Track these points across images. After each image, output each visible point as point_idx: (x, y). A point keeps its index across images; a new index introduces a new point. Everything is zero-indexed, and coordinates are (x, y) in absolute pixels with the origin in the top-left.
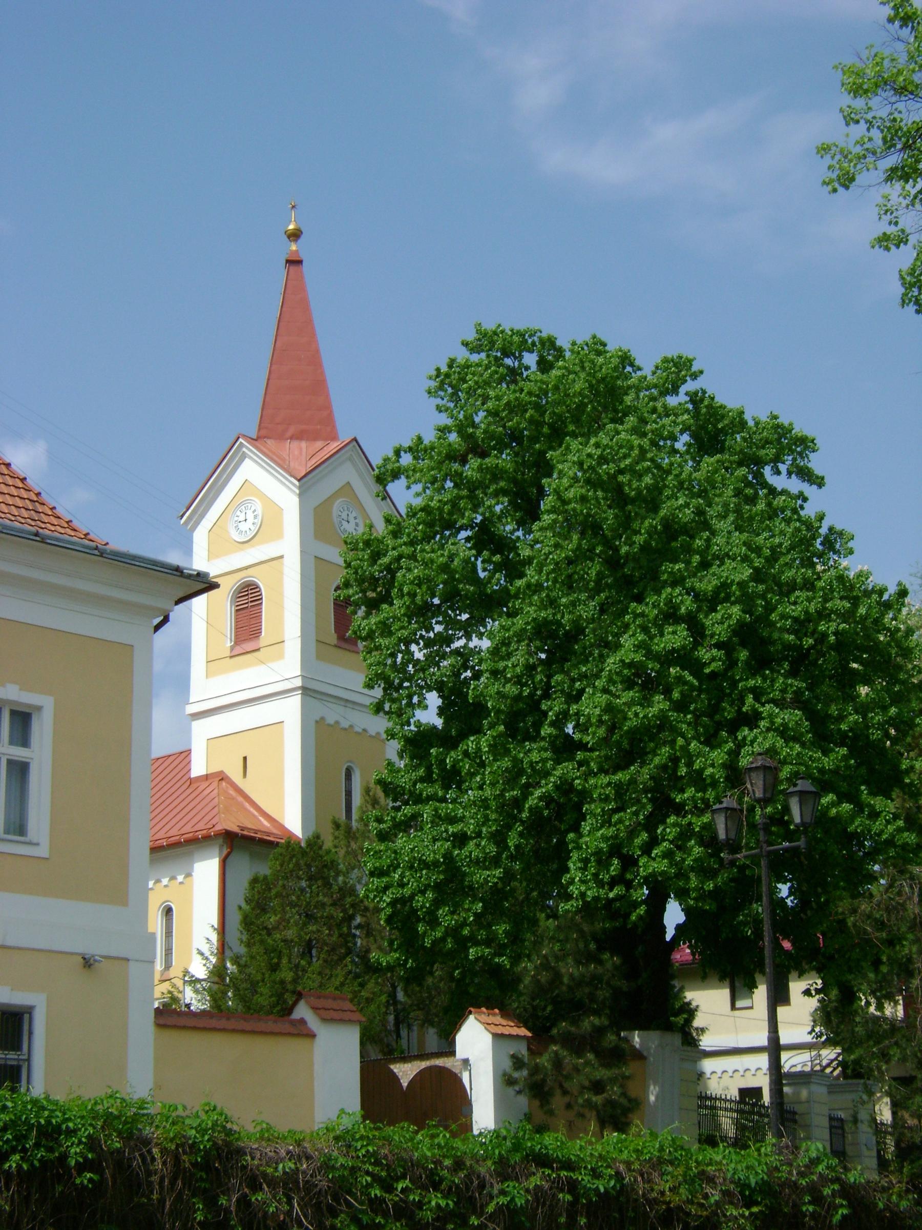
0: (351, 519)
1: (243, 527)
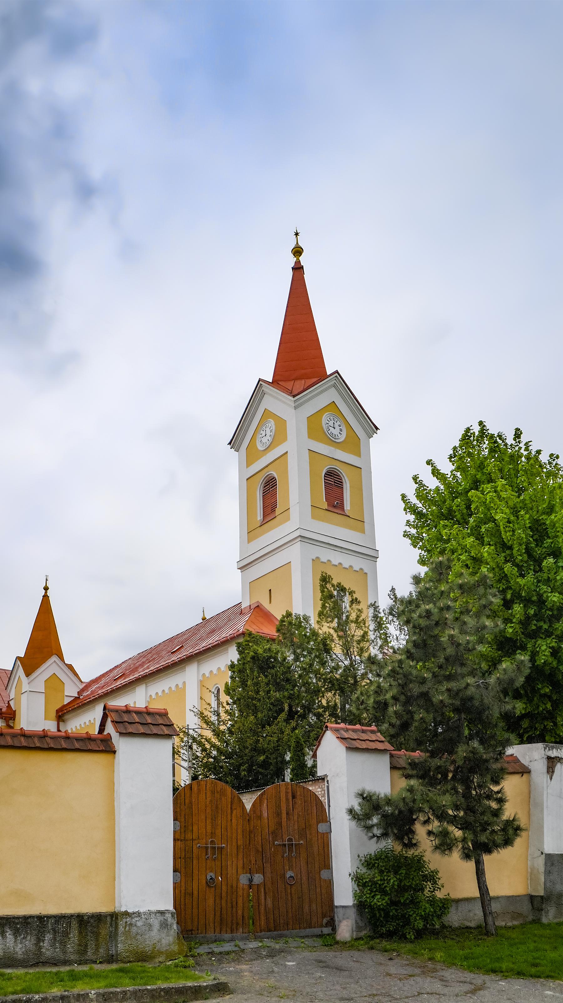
0: (336, 425)
1: (265, 440)
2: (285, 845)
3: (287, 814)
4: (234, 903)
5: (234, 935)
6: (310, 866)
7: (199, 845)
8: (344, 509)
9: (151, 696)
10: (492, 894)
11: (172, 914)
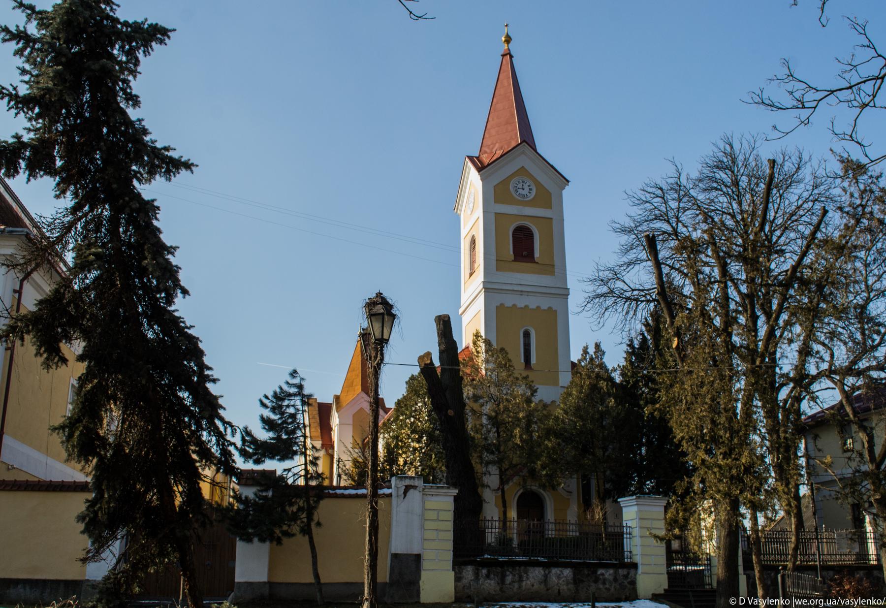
0: (526, 186)
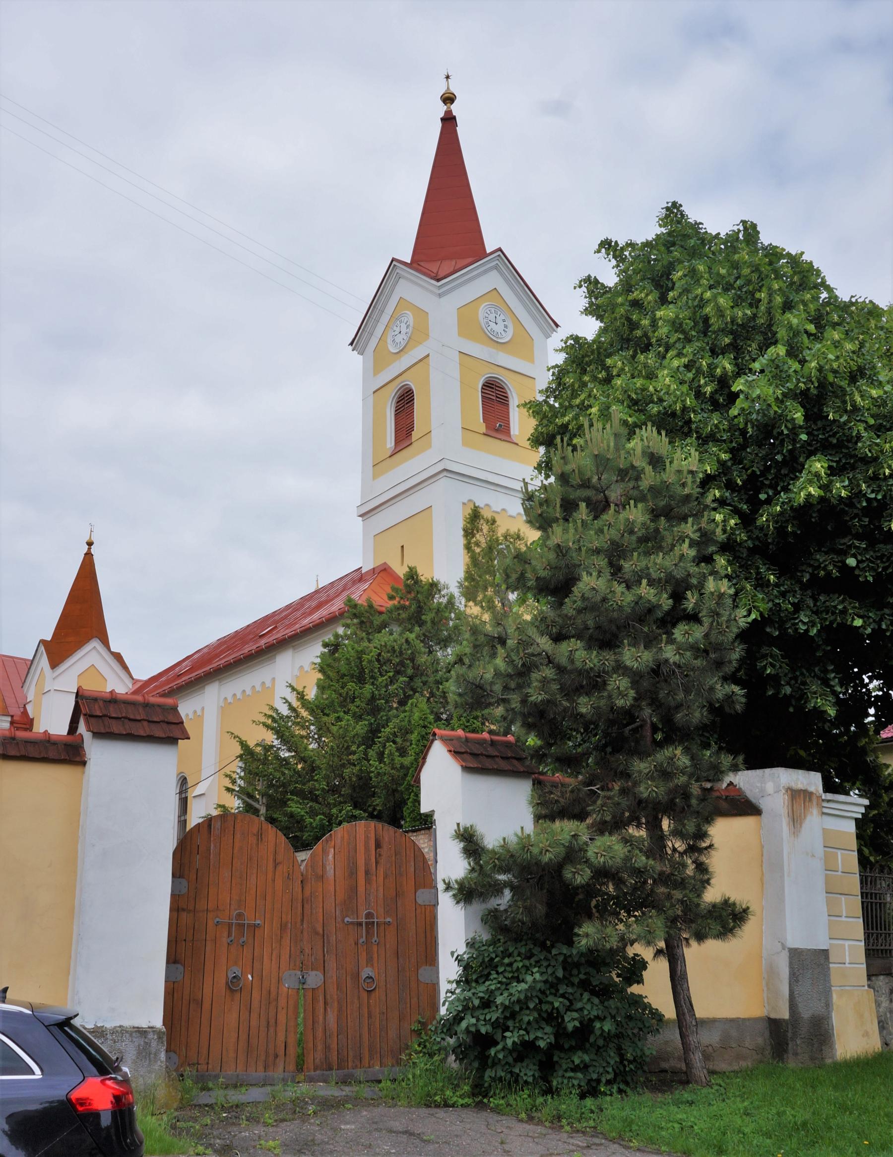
0: (499, 320)
1: (399, 339)
2: (360, 924)
3: (367, 872)
4: (272, 1022)
5: (270, 1074)
6: (401, 960)
7: (218, 920)
8: (509, 433)
9: (226, 699)
10: (700, 1013)
11: (159, 1033)
